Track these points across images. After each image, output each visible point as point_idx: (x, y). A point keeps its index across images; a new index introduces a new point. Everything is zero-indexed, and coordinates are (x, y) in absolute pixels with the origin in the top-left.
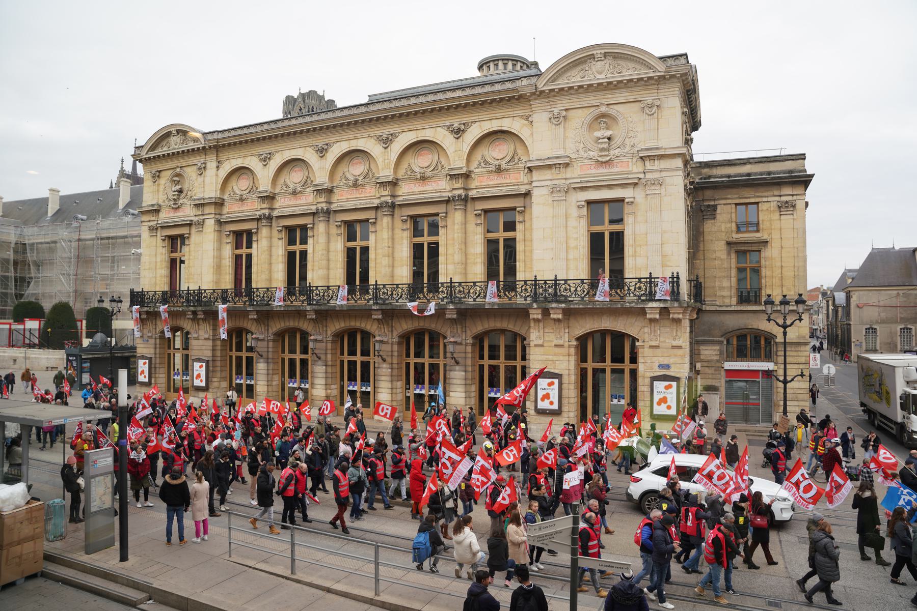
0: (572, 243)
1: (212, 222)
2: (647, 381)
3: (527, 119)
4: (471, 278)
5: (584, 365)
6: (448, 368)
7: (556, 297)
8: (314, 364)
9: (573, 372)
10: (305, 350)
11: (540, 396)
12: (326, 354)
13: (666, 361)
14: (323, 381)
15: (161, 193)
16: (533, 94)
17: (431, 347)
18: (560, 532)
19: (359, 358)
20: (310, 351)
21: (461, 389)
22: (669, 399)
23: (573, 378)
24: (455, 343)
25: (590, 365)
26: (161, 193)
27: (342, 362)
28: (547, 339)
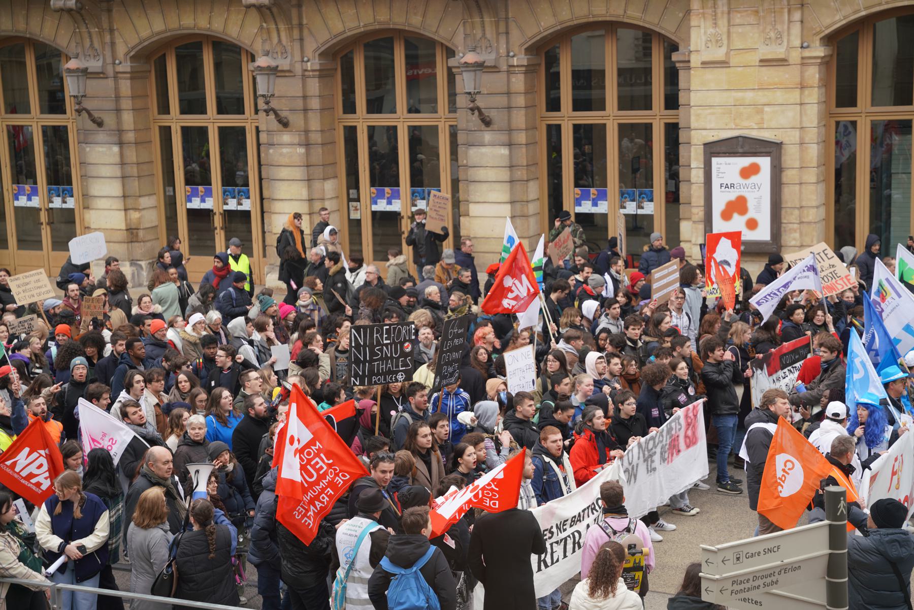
5: (846, 114)
6: (461, 138)
8: (84, 141)
9: (813, 135)
10: (54, 102)
11: (718, 206)
12: (118, 110)
14: (115, 188)
17: (412, 82)
18: (794, 568)
19: (212, 121)
20: (70, 105)
21: (501, 193)
22: (751, 204)
23: (813, 151)
24: (479, 66)
25: (867, 113)
27: (166, 132)
28: (738, 44)
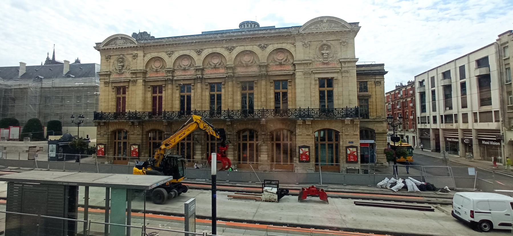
0: (313, 94)
1: (142, 81)
2: (344, 148)
3: (293, 44)
4: (268, 108)
7: (309, 116)
13: (351, 140)
14: (200, 152)
15: (111, 66)
16: (297, 34)
23: (314, 147)
26: (111, 66)
